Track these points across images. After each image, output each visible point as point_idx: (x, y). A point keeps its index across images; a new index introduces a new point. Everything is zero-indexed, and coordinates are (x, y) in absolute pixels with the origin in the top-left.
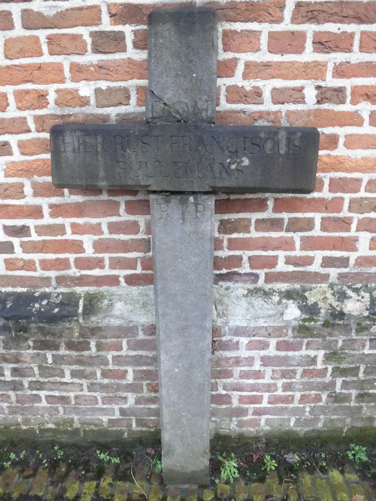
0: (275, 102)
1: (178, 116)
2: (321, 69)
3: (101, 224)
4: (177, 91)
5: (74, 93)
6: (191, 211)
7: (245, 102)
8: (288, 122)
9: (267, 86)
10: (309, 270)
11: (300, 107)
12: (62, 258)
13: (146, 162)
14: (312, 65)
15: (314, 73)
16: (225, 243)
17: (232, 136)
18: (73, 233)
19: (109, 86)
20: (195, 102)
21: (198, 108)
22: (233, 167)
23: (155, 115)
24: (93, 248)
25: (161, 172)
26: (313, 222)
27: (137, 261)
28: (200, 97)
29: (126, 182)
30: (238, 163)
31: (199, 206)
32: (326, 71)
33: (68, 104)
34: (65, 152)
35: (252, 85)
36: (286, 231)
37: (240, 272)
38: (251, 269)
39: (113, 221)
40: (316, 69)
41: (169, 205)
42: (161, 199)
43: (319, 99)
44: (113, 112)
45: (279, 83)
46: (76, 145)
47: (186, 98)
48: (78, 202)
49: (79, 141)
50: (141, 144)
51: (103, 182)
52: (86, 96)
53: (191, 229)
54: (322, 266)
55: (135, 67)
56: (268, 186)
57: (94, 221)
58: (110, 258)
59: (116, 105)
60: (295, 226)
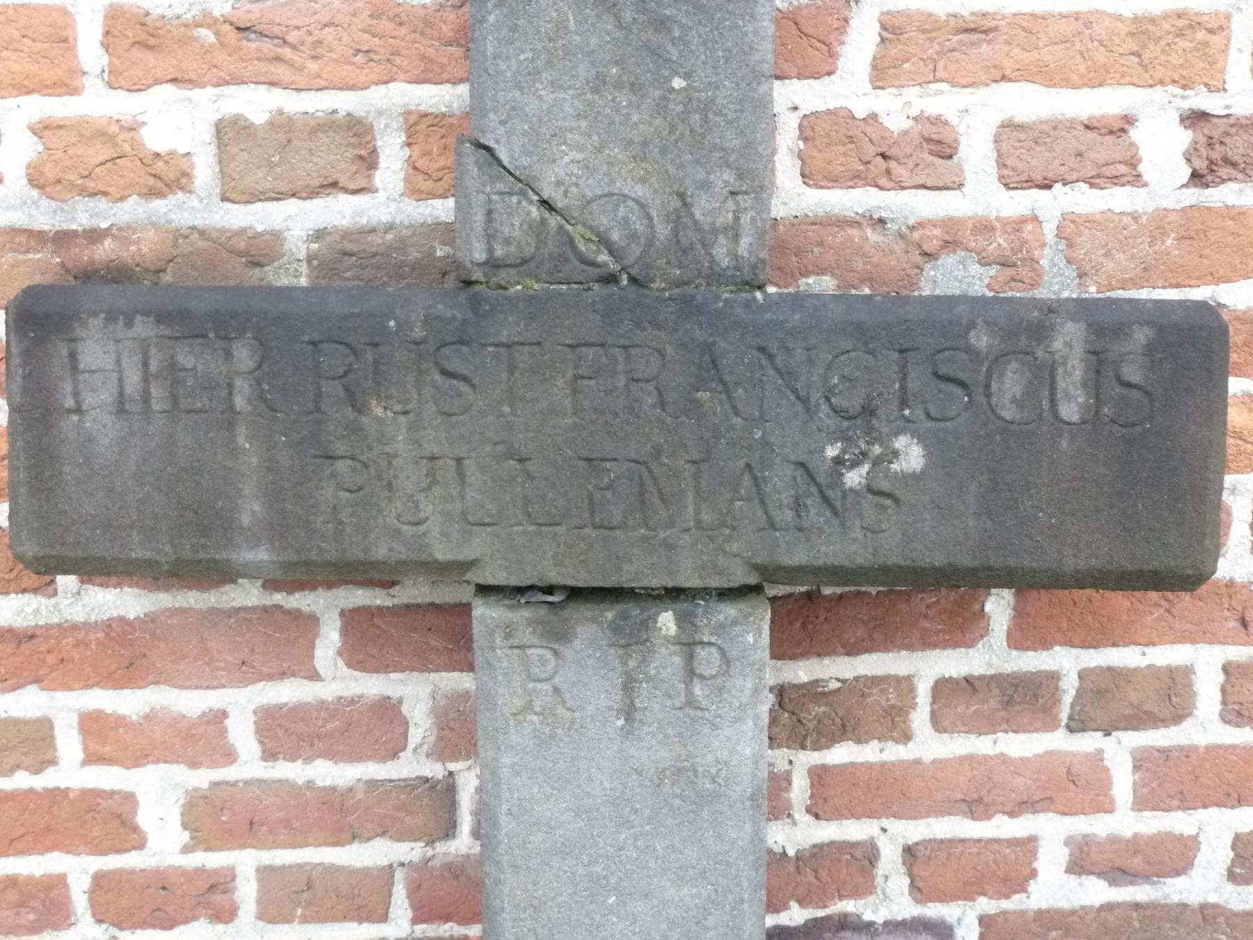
0: (1014, 179)
1: (604, 257)
2: (1206, 44)
3: (224, 714)
4: (599, 150)
5: (117, 141)
6: (664, 675)
7: (883, 181)
8: (1069, 262)
9: (977, 114)
10: (1175, 898)
11: (1119, 199)
12: (30, 879)
13: (459, 460)
14: (1166, 26)
15: (1176, 60)
16: (799, 790)
17: (846, 344)
18: (92, 758)
19: (280, 112)
20: (682, 196)
21: (696, 223)
22: (854, 478)
23: (499, 252)
24: (185, 826)
25: (527, 501)
26: (1189, 686)
27: (390, 883)
28: (701, 175)
29: (366, 550)
30: (876, 462)
31: (702, 653)
32: (1225, 50)
33: (91, 185)
34: (78, 410)
35: (915, 112)
36: (1070, 729)
37: (868, 916)
38: (917, 901)
39: (284, 699)
40: (1182, 43)
41: (566, 651)
42: (529, 622)
43: (1201, 165)
44: (297, 222)
45: (1031, 102)
46: (133, 380)
47: (643, 181)
48: (122, 620)
49: (145, 365)
50: (437, 377)
51: (256, 546)
52: (172, 153)
53: (664, 755)
54: (1232, 877)
55: (403, 31)
56: (1012, 562)
57: (191, 702)
58: (265, 873)
59: (313, 193)
60: (1106, 704)
